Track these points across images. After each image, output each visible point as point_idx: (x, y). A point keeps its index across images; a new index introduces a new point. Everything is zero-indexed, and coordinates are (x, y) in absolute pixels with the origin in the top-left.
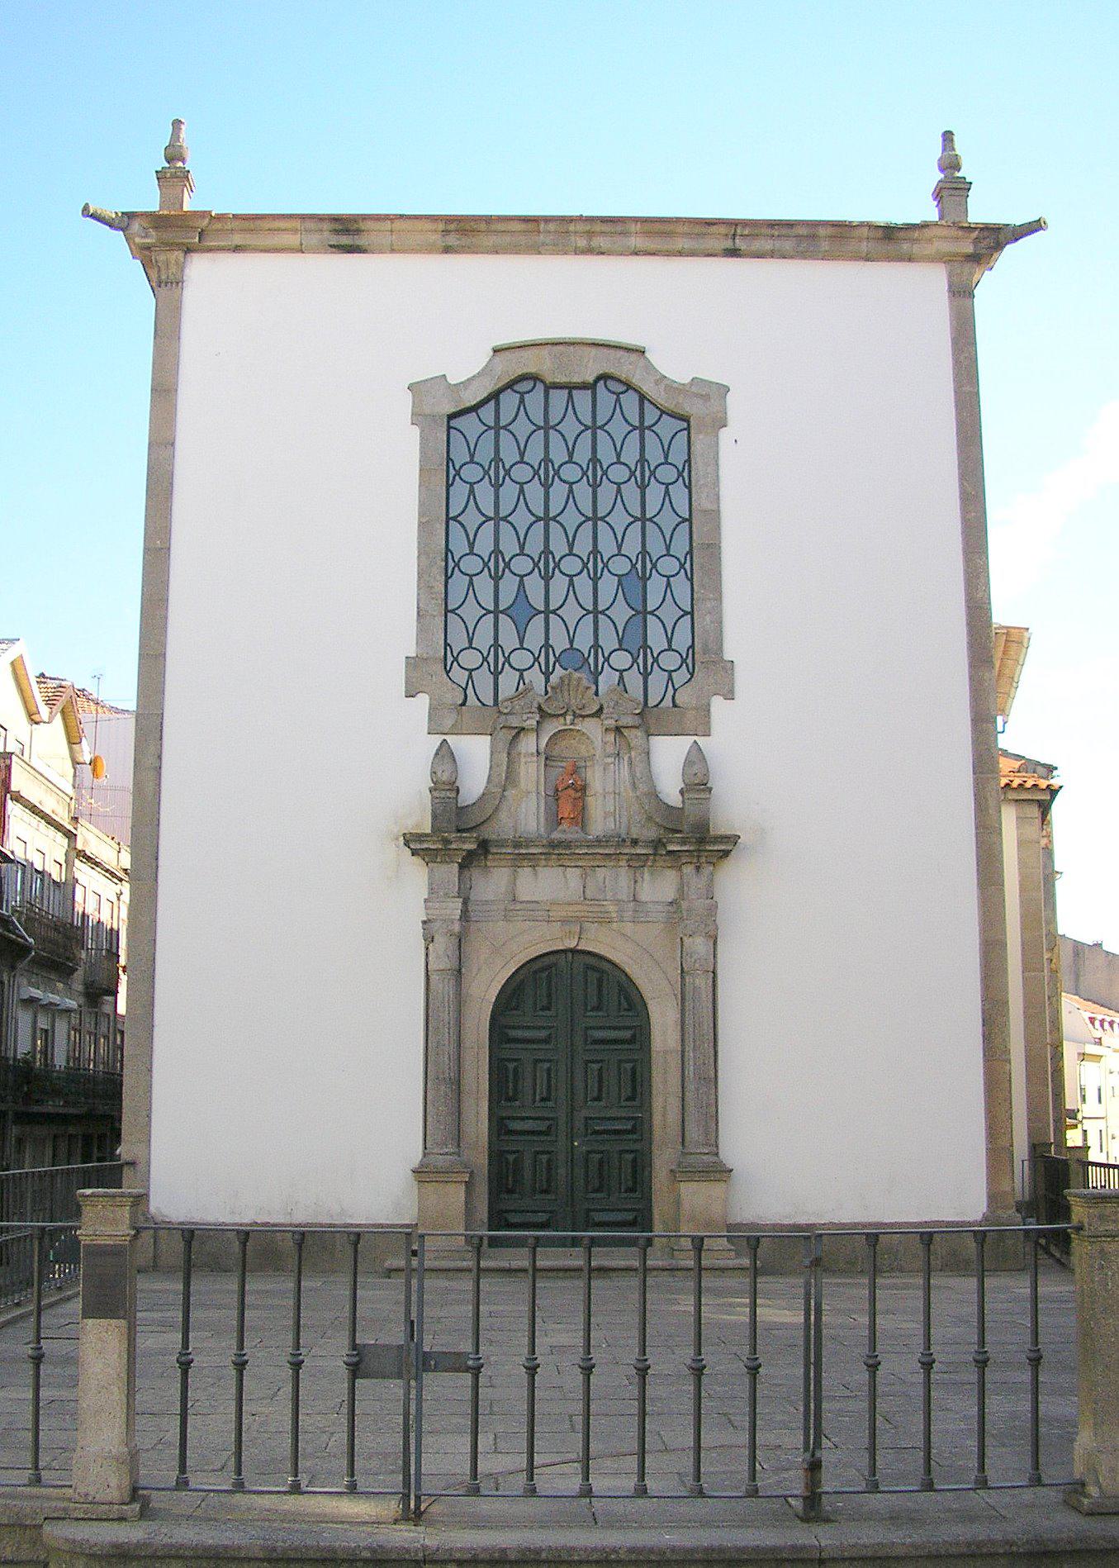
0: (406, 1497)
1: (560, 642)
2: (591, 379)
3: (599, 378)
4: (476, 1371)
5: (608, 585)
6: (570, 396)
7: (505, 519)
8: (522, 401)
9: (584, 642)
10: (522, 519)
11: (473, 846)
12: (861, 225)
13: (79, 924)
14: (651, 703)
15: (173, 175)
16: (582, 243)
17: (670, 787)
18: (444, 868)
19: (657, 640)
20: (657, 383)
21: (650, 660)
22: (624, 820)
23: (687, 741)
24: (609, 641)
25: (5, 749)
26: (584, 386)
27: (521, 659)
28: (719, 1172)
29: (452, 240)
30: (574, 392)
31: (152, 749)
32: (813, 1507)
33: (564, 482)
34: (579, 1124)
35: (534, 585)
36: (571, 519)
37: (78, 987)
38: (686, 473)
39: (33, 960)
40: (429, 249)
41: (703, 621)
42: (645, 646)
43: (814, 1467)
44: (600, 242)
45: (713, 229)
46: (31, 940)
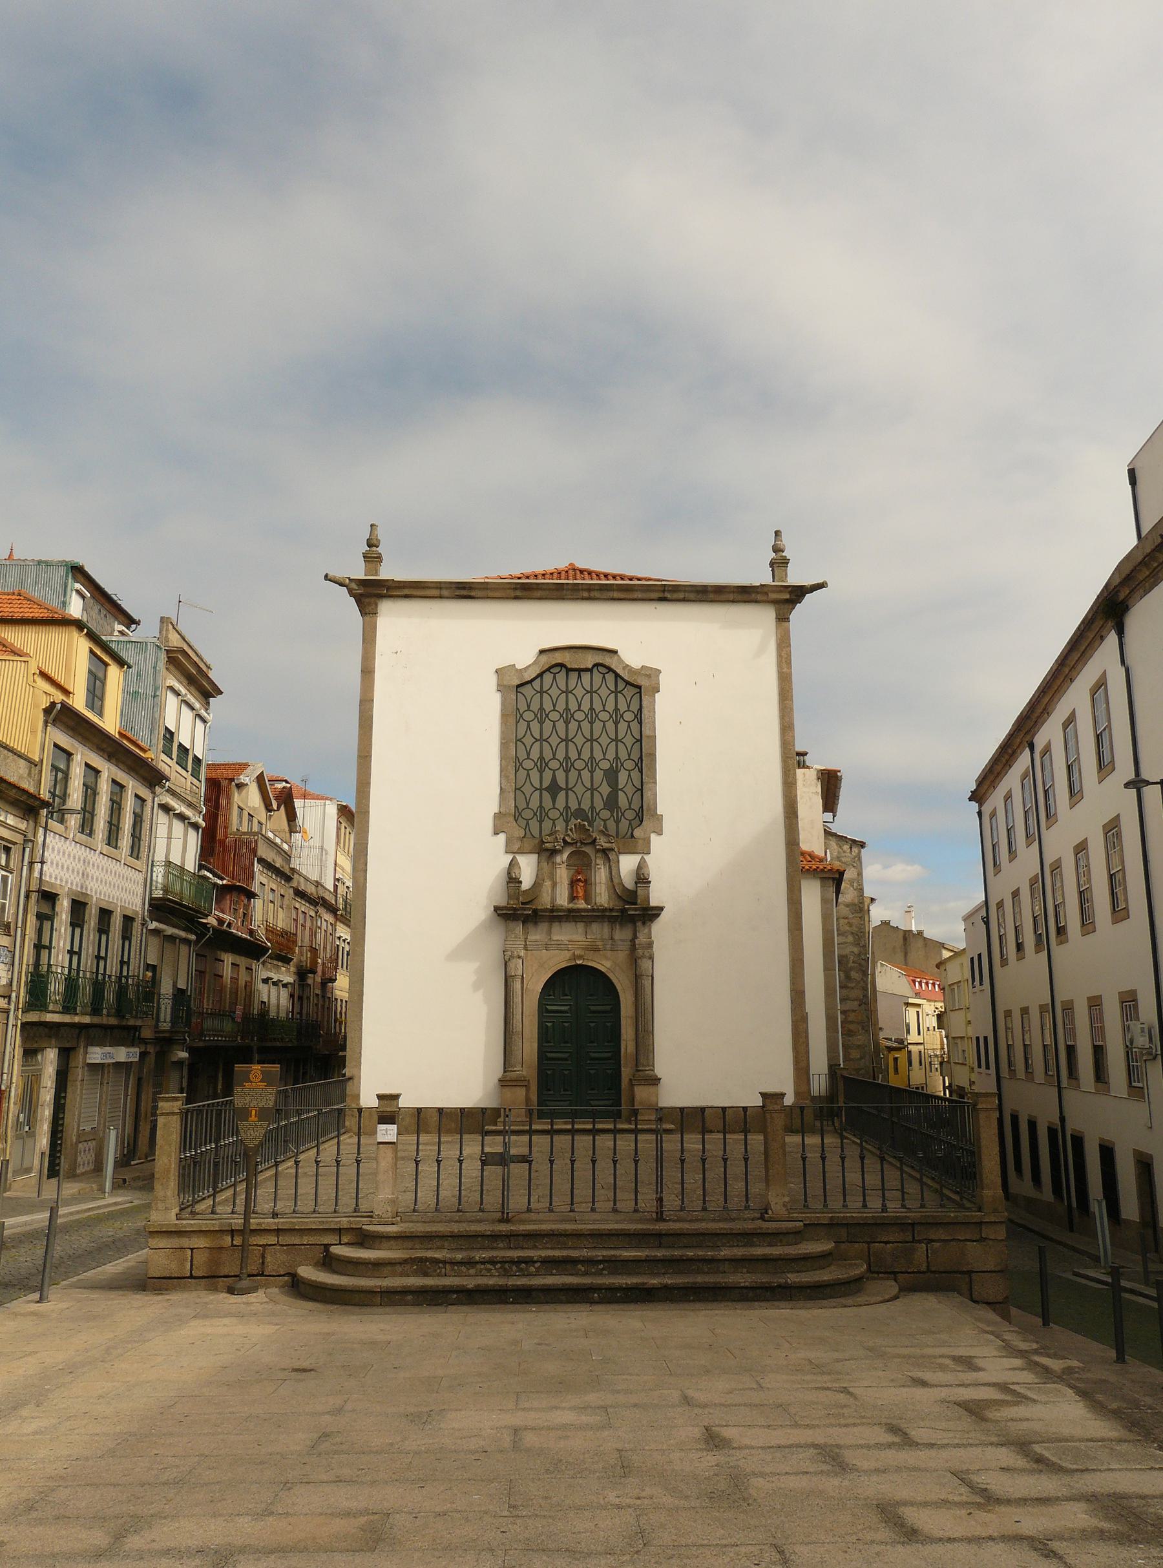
0: (503, 1213)
1: (574, 805)
2: (590, 667)
3: (594, 666)
4: (530, 1162)
5: (598, 775)
6: (579, 675)
17: (628, 881)
20: (624, 668)
23: (637, 858)
24: (599, 804)
25: (573, 1140)
26: (586, 670)
28: (655, 1081)
31: (362, 861)
32: (660, 1217)
33: (576, 721)
37: (293, 969)
38: (639, 717)
39: (270, 957)
41: (647, 794)
43: (660, 1200)
44: (593, 594)
46: (269, 944)
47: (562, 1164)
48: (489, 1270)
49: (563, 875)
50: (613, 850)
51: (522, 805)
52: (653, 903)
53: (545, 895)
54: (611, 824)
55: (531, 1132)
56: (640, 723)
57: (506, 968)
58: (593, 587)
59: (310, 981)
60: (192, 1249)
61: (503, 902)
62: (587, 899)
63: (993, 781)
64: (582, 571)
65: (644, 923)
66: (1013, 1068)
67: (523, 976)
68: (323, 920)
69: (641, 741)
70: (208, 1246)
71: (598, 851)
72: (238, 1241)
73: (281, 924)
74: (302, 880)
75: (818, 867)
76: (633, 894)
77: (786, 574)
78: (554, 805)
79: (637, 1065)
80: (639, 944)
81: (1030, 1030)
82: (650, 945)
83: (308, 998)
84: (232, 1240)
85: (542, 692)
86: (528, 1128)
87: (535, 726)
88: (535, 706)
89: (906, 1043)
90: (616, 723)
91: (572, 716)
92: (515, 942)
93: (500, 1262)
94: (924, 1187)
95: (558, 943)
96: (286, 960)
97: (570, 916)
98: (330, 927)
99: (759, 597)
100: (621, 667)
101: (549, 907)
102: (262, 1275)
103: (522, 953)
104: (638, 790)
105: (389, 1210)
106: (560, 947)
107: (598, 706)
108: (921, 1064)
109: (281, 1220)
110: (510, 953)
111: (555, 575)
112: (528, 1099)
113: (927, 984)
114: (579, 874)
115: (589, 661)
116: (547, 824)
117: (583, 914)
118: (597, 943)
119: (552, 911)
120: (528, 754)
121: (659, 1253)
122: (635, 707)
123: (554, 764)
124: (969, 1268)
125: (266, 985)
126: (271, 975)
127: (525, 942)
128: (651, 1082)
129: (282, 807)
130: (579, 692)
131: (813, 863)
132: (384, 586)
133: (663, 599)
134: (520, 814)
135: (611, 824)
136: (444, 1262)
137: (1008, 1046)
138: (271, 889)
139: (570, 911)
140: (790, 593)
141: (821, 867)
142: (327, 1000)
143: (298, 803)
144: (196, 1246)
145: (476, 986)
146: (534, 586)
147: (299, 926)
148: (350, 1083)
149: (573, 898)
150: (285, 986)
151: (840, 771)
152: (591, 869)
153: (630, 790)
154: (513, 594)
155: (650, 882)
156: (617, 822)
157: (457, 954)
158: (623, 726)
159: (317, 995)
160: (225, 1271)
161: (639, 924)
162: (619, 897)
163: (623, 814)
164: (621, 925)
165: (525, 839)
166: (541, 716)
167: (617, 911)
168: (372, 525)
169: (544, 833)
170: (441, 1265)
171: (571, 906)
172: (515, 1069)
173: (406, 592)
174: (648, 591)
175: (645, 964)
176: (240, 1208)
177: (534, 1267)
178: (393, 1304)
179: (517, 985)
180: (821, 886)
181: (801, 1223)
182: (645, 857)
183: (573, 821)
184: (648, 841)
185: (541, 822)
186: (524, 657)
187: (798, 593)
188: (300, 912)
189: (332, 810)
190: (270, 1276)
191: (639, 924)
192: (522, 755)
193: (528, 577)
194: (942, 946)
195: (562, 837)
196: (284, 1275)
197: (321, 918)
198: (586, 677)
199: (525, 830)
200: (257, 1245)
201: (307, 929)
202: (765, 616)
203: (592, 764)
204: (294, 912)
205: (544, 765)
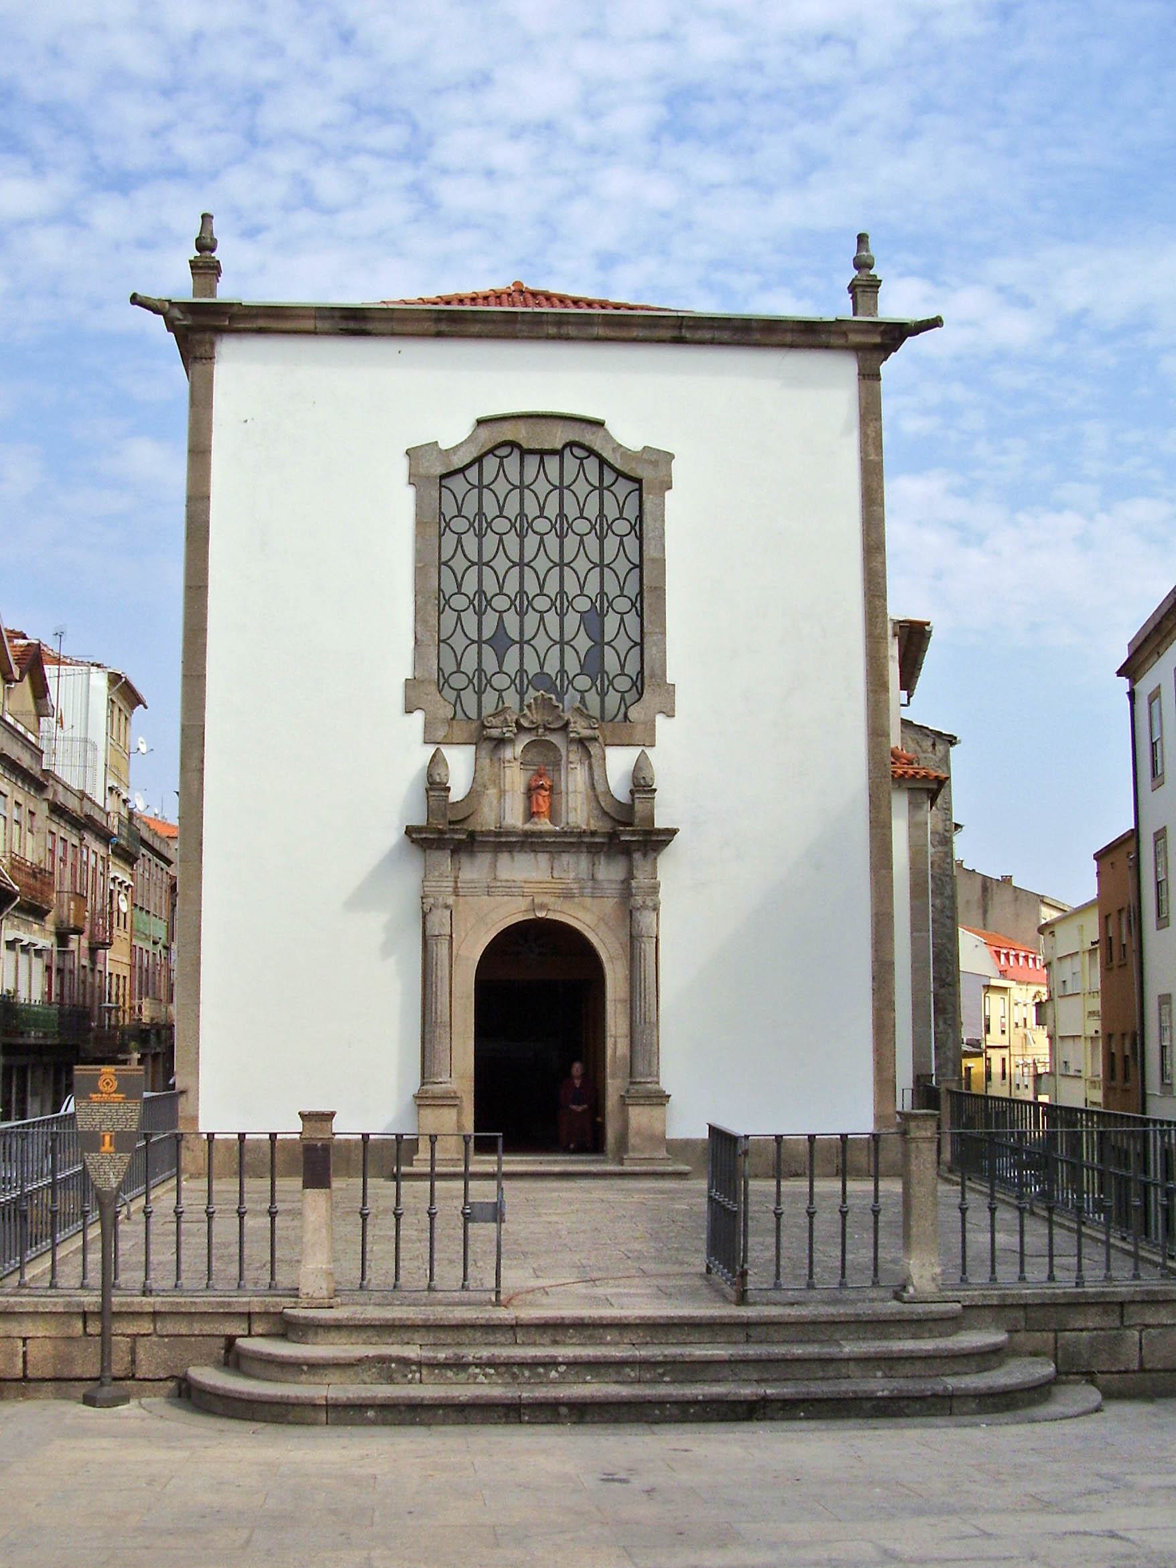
1: (532, 668)
2: (559, 447)
3: (565, 447)
5: (572, 620)
23: (634, 753)
24: (572, 667)
26: (553, 452)
28: (661, 1099)
37: (50, 927)
38: (638, 528)
46: (17, 888)
47: (414, 1227)
48: (476, 1376)
49: (516, 779)
50: (595, 739)
51: (449, 667)
52: (659, 824)
53: (486, 809)
54: (593, 699)
55: (467, 1176)
56: (640, 538)
57: (424, 923)
58: (565, 318)
59: (73, 946)
60: (25, 1339)
61: (419, 820)
62: (553, 816)
63: (1158, 645)
64: (534, 294)
65: (645, 855)
66: (1167, 1081)
67: (451, 936)
68: (90, 851)
69: (640, 567)
70: (47, 1334)
71: (572, 741)
72: (94, 1328)
73: (30, 857)
74: (60, 788)
75: (905, 772)
76: (629, 808)
77: (876, 304)
78: (500, 666)
79: (631, 1076)
80: (638, 888)
81: (1171, 1027)
82: (655, 889)
83: (72, 972)
84: (85, 1328)
85: (481, 487)
87: (470, 542)
88: (470, 509)
89: (983, 1046)
90: (601, 539)
91: (530, 525)
92: (439, 884)
94: (1112, 1251)
95: (508, 884)
96: (37, 912)
97: (529, 842)
98: (100, 863)
99: (834, 340)
100: (610, 447)
101: (493, 828)
102: (133, 1378)
103: (451, 900)
104: (636, 644)
105: (324, 1286)
106: (510, 890)
107: (571, 511)
108: (1004, 1077)
109: (159, 1299)
110: (431, 900)
111: (492, 300)
112: (460, 1126)
113: (1017, 956)
114: (540, 776)
115: (557, 437)
116: (490, 698)
117: (547, 840)
118: (572, 886)
119: (498, 834)
120: (459, 586)
121: (752, 1351)
122: (631, 512)
123: (501, 603)
125: (13, 953)
126: (20, 934)
127: (456, 882)
128: (655, 1101)
129: (26, 678)
130: (542, 487)
131: (898, 765)
132: (224, 314)
133: (679, 341)
134: (446, 681)
135: (593, 699)
136: (420, 1364)
137: (1163, 1048)
138: (16, 802)
139: (527, 834)
140: (883, 333)
141: (911, 772)
142: (98, 975)
143: (50, 670)
144: (30, 1335)
145: (386, 950)
146: (469, 316)
147: (57, 861)
148: (182, 1100)
149: (530, 815)
150: (39, 953)
151: (928, 624)
152: (559, 770)
153: (623, 644)
154: (433, 328)
155: (655, 790)
156: (603, 694)
157: (359, 901)
158: (611, 543)
159: (84, 967)
160: (78, 1371)
161: (637, 856)
162: (605, 813)
163: (611, 683)
164: (609, 856)
165: (454, 722)
166: (480, 524)
167: (604, 834)
168: (204, 216)
169: (485, 713)
170: (414, 1368)
171: (528, 827)
172: (440, 1080)
173: (261, 323)
174: (655, 326)
175: (646, 919)
176: (95, 1278)
177: (557, 1371)
178: (338, 1423)
179: (442, 950)
180: (910, 803)
181: (959, 1306)
182: (648, 751)
183: (531, 694)
185: (480, 693)
187: (896, 334)
188: (58, 839)
189: (99, 681)
190: (145, 1380)
191: (637, 856)
192: (449, 587)
193: (448, 303)
194: (1042, 900)
195: (515, 717)
196: (165, 1380)
197: (88, 848)
198: (552, 463)
199: (455, 706)
200: (124, 1335)
201: (69, 865)
202: (845, 368)
203: (562, 603)
204: (49, 838)
205: (484, 603)
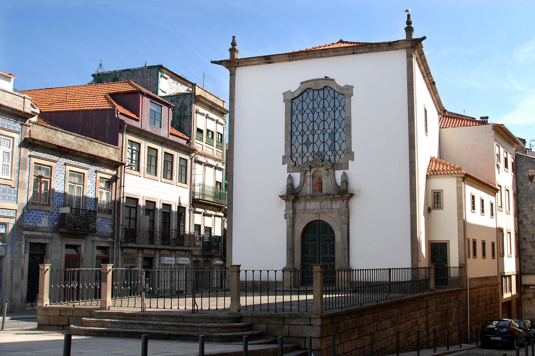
1: (316, 150)
2: (322, 88)
5: (327, 136)
7: (304, 122)
8: (308, 94)
9: (321, 150)
10: (308, 122)
11: (294, 198)
12: (382, 43)
13: (388, 281)
14: (336, 163)
15: (233, 50)
16: (319, 55)
17: (339, 181)
18: (289, 203)
19: (337, 148)
21: (336, 153)
22: (329, 190)
23: (343, 171)
24: (327, 149)
26: (321, 89)
27: (308, 154)
29: (291, 58)
30: (319, 91)
34: (321, 259)
35: (311, 137)
36: (319, 121)
40: (286, 61)
42: (335, 150)
45: (348, 49)
86: (297, 289)
93: (125, 324)
124: (305, 336)
184: (347, 164)
186: (294, 87)
